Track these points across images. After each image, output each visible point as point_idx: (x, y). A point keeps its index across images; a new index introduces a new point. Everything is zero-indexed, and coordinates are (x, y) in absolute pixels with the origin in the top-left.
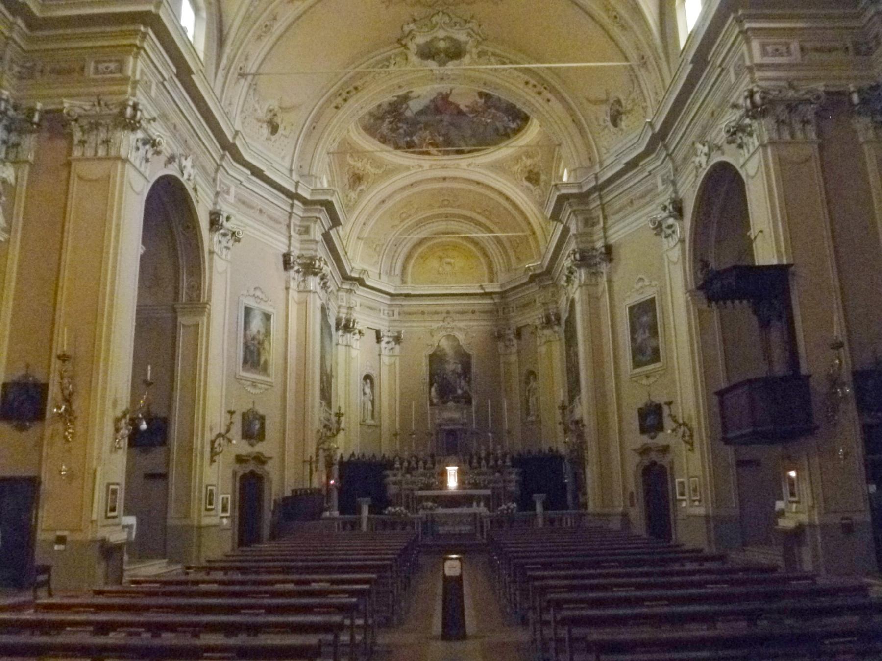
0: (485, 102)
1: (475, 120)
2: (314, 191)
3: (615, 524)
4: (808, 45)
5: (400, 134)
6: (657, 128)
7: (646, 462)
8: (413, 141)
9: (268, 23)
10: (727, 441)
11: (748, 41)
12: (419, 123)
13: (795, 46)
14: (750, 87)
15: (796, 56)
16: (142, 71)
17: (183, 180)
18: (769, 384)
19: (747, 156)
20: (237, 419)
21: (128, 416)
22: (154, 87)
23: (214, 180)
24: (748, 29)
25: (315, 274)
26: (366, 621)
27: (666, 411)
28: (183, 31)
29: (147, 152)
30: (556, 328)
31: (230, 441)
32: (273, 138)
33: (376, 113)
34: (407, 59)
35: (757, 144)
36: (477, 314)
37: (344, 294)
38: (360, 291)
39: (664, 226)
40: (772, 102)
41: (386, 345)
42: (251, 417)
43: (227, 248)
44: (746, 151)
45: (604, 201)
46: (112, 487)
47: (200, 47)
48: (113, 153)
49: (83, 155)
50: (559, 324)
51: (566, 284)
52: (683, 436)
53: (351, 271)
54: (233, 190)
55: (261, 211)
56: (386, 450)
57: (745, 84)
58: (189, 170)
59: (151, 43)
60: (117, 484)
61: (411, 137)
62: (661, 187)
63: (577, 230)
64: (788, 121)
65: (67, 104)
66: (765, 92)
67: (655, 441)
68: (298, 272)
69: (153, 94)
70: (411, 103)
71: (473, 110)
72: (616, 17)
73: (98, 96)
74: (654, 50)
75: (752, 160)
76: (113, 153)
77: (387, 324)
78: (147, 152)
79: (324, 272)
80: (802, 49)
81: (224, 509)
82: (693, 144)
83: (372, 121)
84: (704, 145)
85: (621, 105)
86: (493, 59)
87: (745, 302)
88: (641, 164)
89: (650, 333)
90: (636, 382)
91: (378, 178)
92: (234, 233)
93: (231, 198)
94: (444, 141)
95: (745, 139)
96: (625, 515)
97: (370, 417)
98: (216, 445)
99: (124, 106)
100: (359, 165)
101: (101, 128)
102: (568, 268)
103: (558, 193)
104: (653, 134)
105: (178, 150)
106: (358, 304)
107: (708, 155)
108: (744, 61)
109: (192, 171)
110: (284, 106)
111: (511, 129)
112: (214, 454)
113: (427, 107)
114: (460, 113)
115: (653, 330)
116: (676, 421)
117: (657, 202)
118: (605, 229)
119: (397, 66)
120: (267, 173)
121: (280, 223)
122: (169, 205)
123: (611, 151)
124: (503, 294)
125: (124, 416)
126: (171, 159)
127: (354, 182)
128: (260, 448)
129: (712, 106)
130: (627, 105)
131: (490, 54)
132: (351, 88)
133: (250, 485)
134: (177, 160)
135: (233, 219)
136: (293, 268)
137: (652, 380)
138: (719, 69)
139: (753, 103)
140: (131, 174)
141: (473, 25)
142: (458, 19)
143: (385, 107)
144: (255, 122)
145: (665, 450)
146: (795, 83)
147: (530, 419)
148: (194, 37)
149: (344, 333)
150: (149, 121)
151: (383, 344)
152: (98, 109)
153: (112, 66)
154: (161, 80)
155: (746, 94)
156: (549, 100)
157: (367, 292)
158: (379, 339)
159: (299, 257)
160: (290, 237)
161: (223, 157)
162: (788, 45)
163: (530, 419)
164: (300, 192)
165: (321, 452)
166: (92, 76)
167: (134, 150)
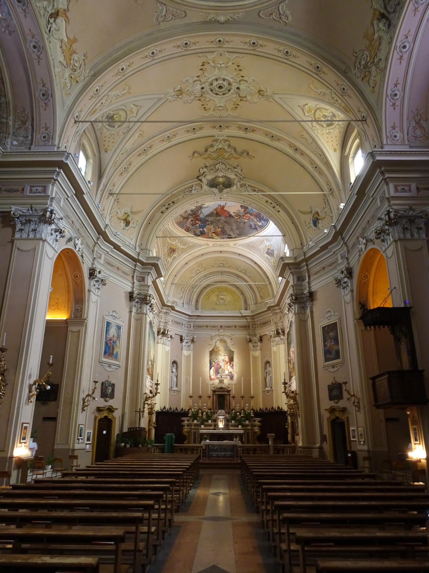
0: (244, 211)
1: (238, 220)
2: (148, 258)
3: (316, 454)
4: (421, 186)
5: (197, 227)
6: (338, 228)
7: (333, 417)
8: (204, 231)
9: (126, 166)
10: (378, 407)
11: (387, 184)
12: (208, 221)
13: (413, 186)
14: (388, 209)
15: (414, 192)
16: (56, 192)
17: (76, 251)
18: (401, 373)
19: (387, 246)
20: (99, 386)
21: (37, 384)
22: (62, 200)
23: (93, 251)
24: (388, 177)
25: (147, 304)
26: (166, 506)
27: (344, 386)
28: (80, 170)
29: (57, 236)
30: (282, 337)
31: (94, 398)
32: (127, 228)
33: (184, 215)
34: (202, 187)
35: (392, 240)
36: (237, 328)
37: (163, 315)
38: (172, 313)
39: (342, 282)
40: (400, 217)
41: (186, 344)
42: (107, 385)
43: (98, 288)
44: (386, 243)
45: (309, 267)
46: (24, 425)
47: (89, 178)
48: (38, 236)
49: (21, 237)
50: (284, 334)
51: (287, 313)
52: (354, 403)
53: (167, 302)
54: (103, 256)
55: (118, 268)
56: (183, 404)
57: (386, 207)
58: (79, 246)
59: (62, 178)
60: (28, 424)
61: (203, 228)
62: (340, 261)
63: (294, 283)
64: (409, 228)
65: (13, 208)
66: (396, 211)
67: (338, 405)
68: (137, 302)
69: (62, 205)
70: (203, 210)
71: (238, 215)
72: (316, 167)
73: (31, 205)
74: (337, 185)
75: (389, 249)
76: (38, 236)
77: (186, 332)
78: (57, 236)
79: (152, 302)
80: (418, 188)
81: (88, 439)
82: (358, 238)
83: (182, 219)
84: (363, 239)
85: (319, 215)
86: (249, 189)
87: (386, 327)
88: (329, 247)
89: (334, 342)
90: (327, 369)
91: (184, 251)
92: (102, 280)
93: (102, 261)
94: (221, 231)
95: (386, 237)
96: (321, 448)
97: (175, 386)
98: (86, 400)
99: (45, 211)
100: (174, 243)
101: (32, 223)
102: (288, 304)
103: (283, 263)
104: (335, 232)
105: (73, 235)
106: (171, 321)
107: (366, 244)
108: (385, 195)
109: (81, 246)
110: (132, 211)
111: (258, 225)
112: (84, 406)
113: (212, 213)
114: (230, 216)
115: (336, 339)
116: (349, 394)
117: (339, 268)
118: (309, 283)
119: (196, 191)
120: (122, 248)
121: (129, 275)
122: (68, 260)
123: (313, 240)
124: (252, 317)
125: (35, 384)
126: (70, 240)
127: (171, 252)
128: (111, 403)
129: (368, 218)
130: (322, 215)
131: (247, 185)
132: (171, 202)
133: (104, 423)
134: (73, 240)
135: (102, 272)
136: (135, 300)
137: (336, 369)
138: (372, 198)
139: (389, 217)
140: (48, 248)
141: (238, 170)
142: (230, 167)
143: (189, 212)
144: (117, 219)
145: (344, 410)
146: (414, 207)
147: (267, 389)
148: (85, 173)
149: (162, 336)
150: (59, 219)
151: (184, 343)
152: (31, 212)
153: (40, 189)
154: (67, 197)
155: (386, 213)
156: (279, 211)
157: (176, 314)
158: (182, 340)
159: (138, 294)
160: (133, 283)
161: (98, 239)
162: (409, 186)
163: (267, 389)
164: (140, 258)
165: (146, 405)
166: (28, 194)
167: (50, 235)
